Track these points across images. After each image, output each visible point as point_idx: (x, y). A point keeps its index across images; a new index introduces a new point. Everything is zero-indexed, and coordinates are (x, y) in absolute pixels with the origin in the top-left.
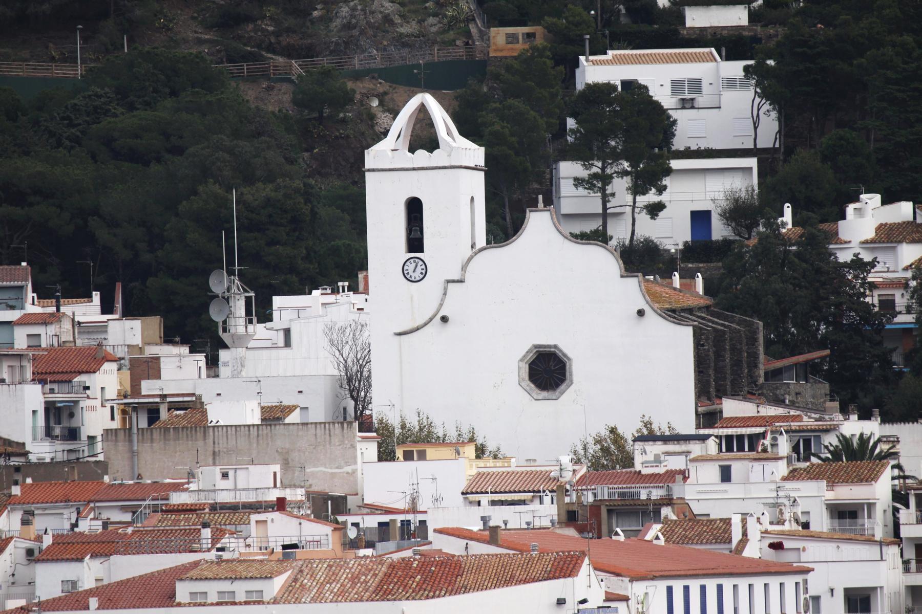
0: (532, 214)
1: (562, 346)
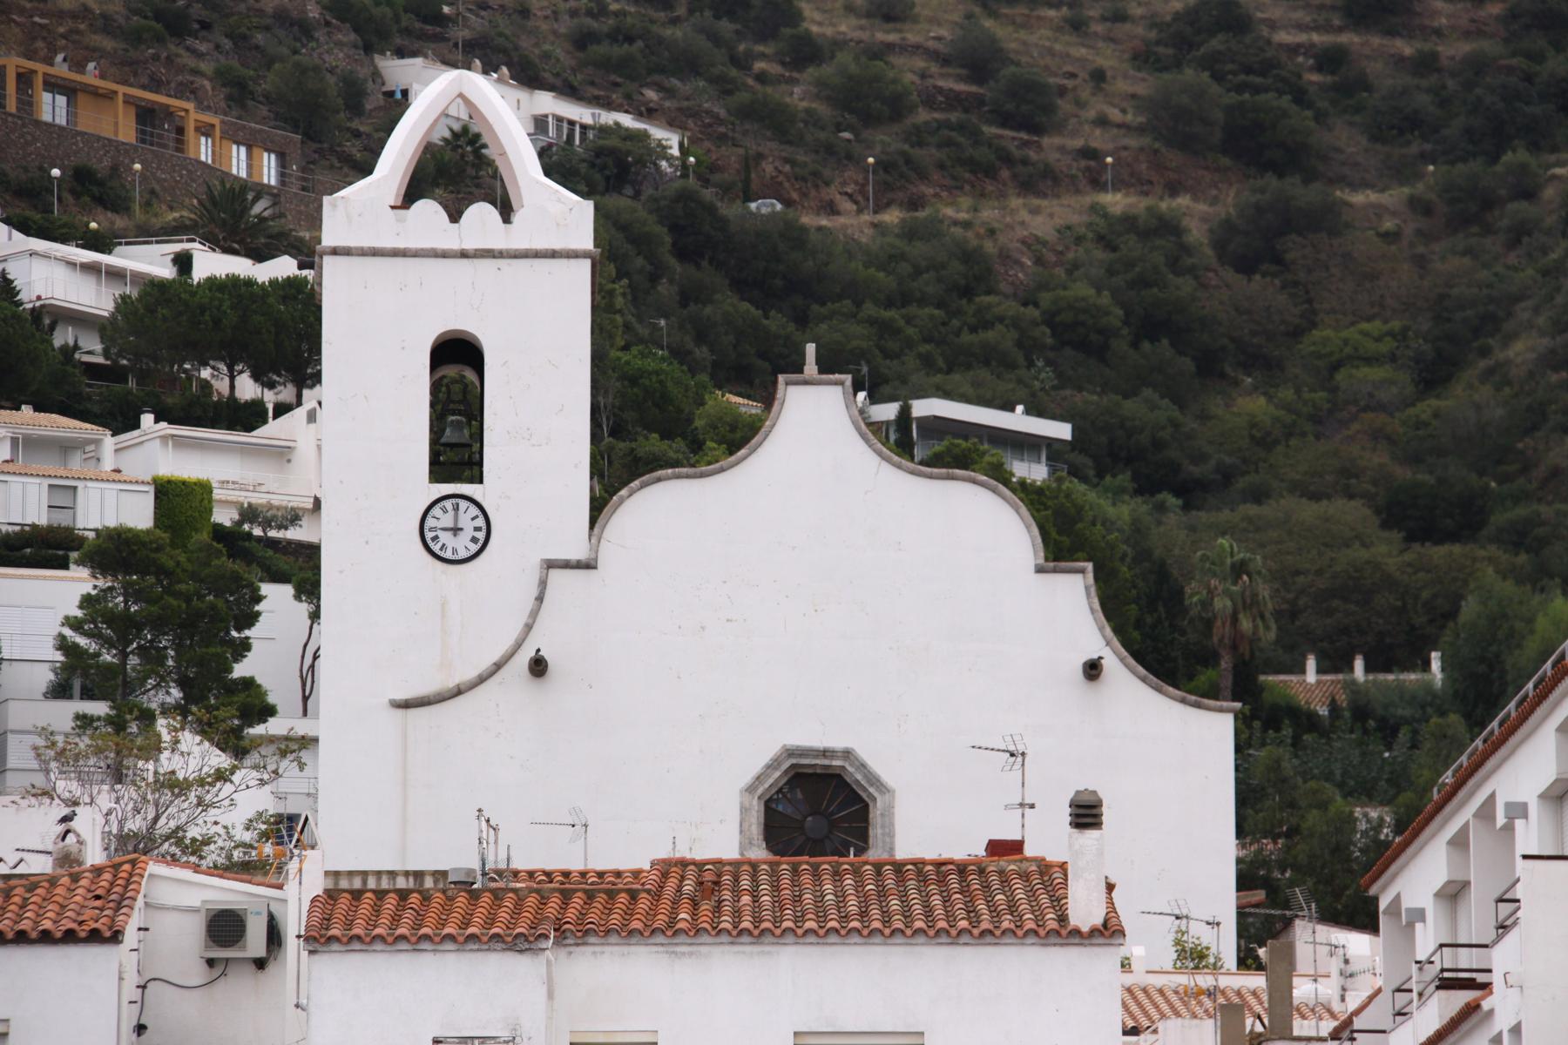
0: (792, 390)
1: (865, 753)
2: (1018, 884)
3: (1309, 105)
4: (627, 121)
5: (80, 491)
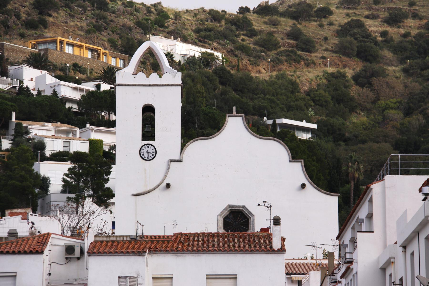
0: (230, 118)
1: (248, 207)
2: (262, 239)
3: (379, 46)
4: (209, 51)
5: (71, 143)
